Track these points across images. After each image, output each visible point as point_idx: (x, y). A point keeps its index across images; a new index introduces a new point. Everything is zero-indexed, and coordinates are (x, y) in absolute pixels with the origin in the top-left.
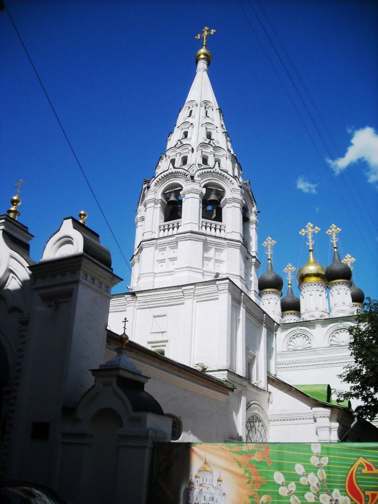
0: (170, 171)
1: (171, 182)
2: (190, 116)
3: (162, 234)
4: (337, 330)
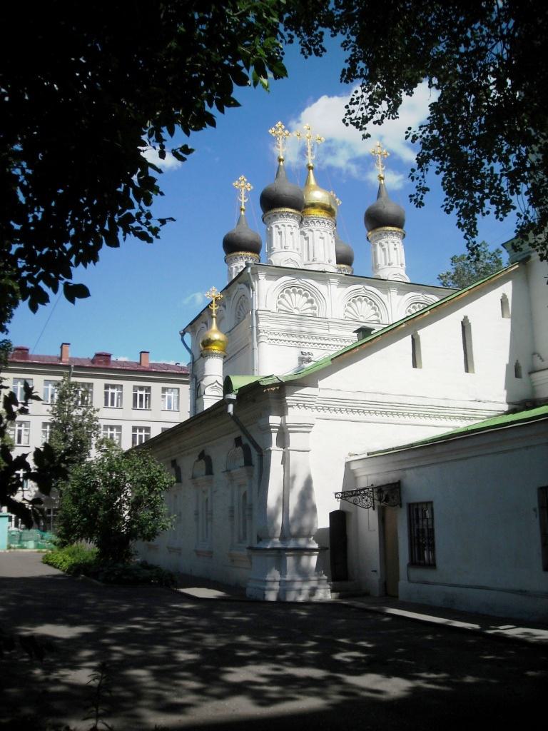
4: (416, 303)
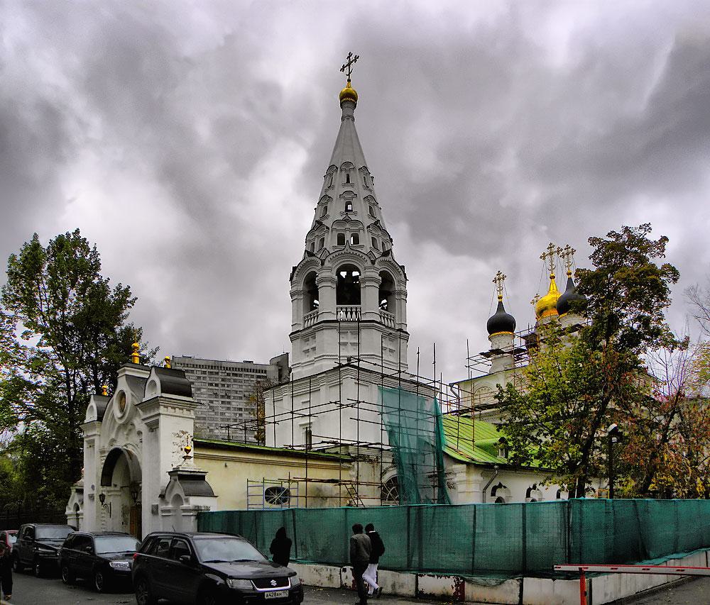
0: (306, 260)
1: (310, 271)
2: (348, 181)
3: (308, 324)
